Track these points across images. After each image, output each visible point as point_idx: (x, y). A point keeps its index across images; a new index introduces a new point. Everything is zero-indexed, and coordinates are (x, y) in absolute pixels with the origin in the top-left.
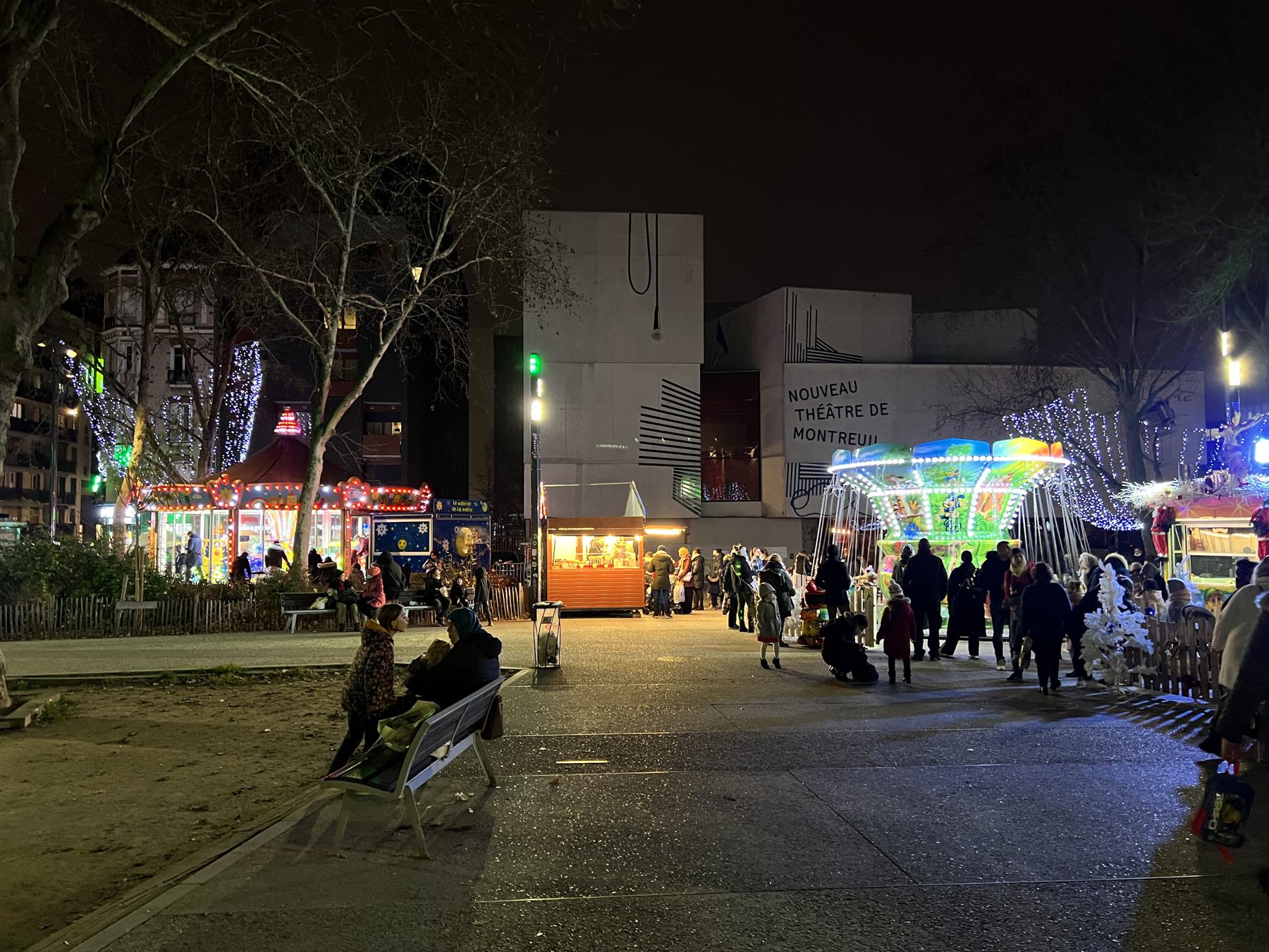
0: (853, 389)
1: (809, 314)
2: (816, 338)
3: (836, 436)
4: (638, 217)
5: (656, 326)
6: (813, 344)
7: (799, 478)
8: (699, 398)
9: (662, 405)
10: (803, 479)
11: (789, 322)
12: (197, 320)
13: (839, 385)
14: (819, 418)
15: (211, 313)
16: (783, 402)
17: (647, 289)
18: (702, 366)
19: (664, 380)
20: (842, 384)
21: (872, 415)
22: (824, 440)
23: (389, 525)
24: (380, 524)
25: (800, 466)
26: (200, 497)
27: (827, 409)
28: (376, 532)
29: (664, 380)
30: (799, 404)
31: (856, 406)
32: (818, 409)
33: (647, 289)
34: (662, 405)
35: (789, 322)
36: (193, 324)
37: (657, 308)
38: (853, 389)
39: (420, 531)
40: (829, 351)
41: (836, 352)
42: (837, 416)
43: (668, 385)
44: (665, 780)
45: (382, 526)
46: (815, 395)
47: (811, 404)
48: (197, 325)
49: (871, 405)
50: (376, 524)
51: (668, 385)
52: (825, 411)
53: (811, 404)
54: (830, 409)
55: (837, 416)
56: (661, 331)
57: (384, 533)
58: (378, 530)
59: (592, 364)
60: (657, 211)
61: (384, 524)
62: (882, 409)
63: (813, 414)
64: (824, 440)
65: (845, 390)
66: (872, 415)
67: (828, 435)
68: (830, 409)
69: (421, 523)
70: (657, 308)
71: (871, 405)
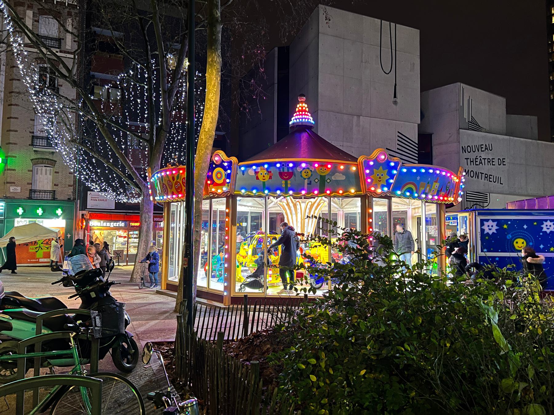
0: (491, 149)
1: (469, 100)
2: (472, 116)
3: (483, 175)
4: (386, 23)
5: (395, 97)
6: (470, 120)
7: (467, 201)
8: (417, 146)
9: (398, 149)
10: (468, 201)
11: (461, 105)
12: (62, 45)
13: (484, 145)
14: (476, 165)
15: (75, 41)
16: (459, 153)
17: (390, 71)
18: (418, 125)
19: (398, 132)
20: (486, 145)
21: (499, 165)
22: (478, 178)
23: (500, 223)
24: (487, 220)
25: (467, 193)
26: (343, 178)
27: (479, 159)
28: (482, 231)
29: (398, 132)
30: (466, 155)
31: (492, 159)
32: (475, 159)
33: (390, 71)
34: (398, 149)
35: (461, 105)
36: (59, 47)
37: (396, 85)
38: (491, 149)
39: (545, 229)
40: (477, 125)
41: (479, 126)
42: (483, 164)
43: (401, 137)
44: (319, 387)
45: (490, 223)
46: (474, 150)
47: (472, 156)
48: (62, 49)
49: (499, 159)
50: (482, 221)
51: (401, 137)
52: (478, 160)
53: (472, 156)
54: (480, 159)
55: (483, 164)
56: (398, 100)
57: (494, 230)
58: (485, 228)
59: (359, 116)
60: (396, 22)
61: (493, 220)
62: (502, 162)
63: (473, 162)
64: (478, 178)
65: (487, 149)
66: (499, 165)
67: (480, 175)
68: (480, 159)
69: (546, 220)
70: (396, 85)
71: (499, 159)
